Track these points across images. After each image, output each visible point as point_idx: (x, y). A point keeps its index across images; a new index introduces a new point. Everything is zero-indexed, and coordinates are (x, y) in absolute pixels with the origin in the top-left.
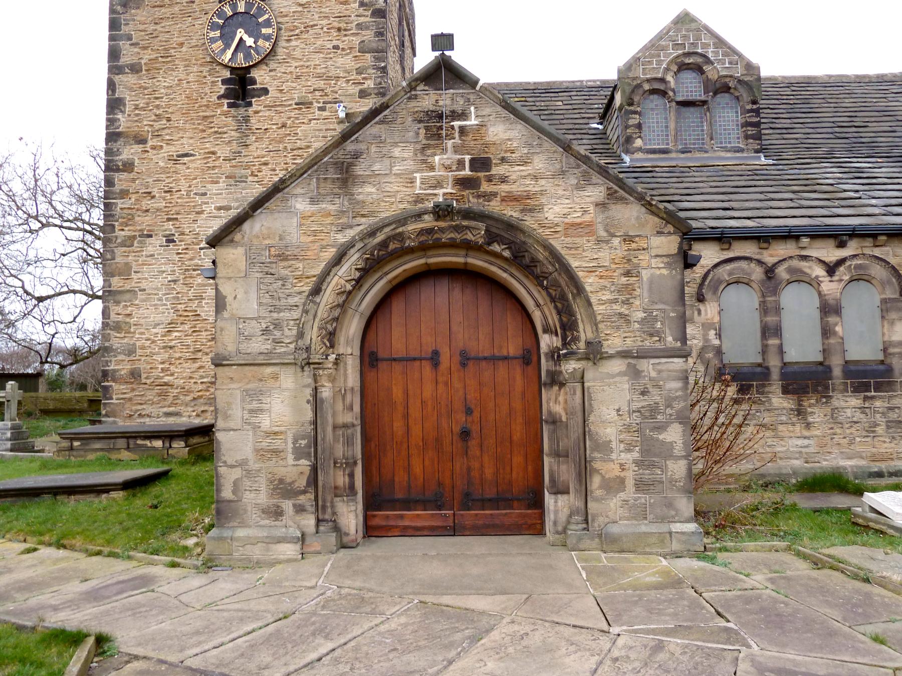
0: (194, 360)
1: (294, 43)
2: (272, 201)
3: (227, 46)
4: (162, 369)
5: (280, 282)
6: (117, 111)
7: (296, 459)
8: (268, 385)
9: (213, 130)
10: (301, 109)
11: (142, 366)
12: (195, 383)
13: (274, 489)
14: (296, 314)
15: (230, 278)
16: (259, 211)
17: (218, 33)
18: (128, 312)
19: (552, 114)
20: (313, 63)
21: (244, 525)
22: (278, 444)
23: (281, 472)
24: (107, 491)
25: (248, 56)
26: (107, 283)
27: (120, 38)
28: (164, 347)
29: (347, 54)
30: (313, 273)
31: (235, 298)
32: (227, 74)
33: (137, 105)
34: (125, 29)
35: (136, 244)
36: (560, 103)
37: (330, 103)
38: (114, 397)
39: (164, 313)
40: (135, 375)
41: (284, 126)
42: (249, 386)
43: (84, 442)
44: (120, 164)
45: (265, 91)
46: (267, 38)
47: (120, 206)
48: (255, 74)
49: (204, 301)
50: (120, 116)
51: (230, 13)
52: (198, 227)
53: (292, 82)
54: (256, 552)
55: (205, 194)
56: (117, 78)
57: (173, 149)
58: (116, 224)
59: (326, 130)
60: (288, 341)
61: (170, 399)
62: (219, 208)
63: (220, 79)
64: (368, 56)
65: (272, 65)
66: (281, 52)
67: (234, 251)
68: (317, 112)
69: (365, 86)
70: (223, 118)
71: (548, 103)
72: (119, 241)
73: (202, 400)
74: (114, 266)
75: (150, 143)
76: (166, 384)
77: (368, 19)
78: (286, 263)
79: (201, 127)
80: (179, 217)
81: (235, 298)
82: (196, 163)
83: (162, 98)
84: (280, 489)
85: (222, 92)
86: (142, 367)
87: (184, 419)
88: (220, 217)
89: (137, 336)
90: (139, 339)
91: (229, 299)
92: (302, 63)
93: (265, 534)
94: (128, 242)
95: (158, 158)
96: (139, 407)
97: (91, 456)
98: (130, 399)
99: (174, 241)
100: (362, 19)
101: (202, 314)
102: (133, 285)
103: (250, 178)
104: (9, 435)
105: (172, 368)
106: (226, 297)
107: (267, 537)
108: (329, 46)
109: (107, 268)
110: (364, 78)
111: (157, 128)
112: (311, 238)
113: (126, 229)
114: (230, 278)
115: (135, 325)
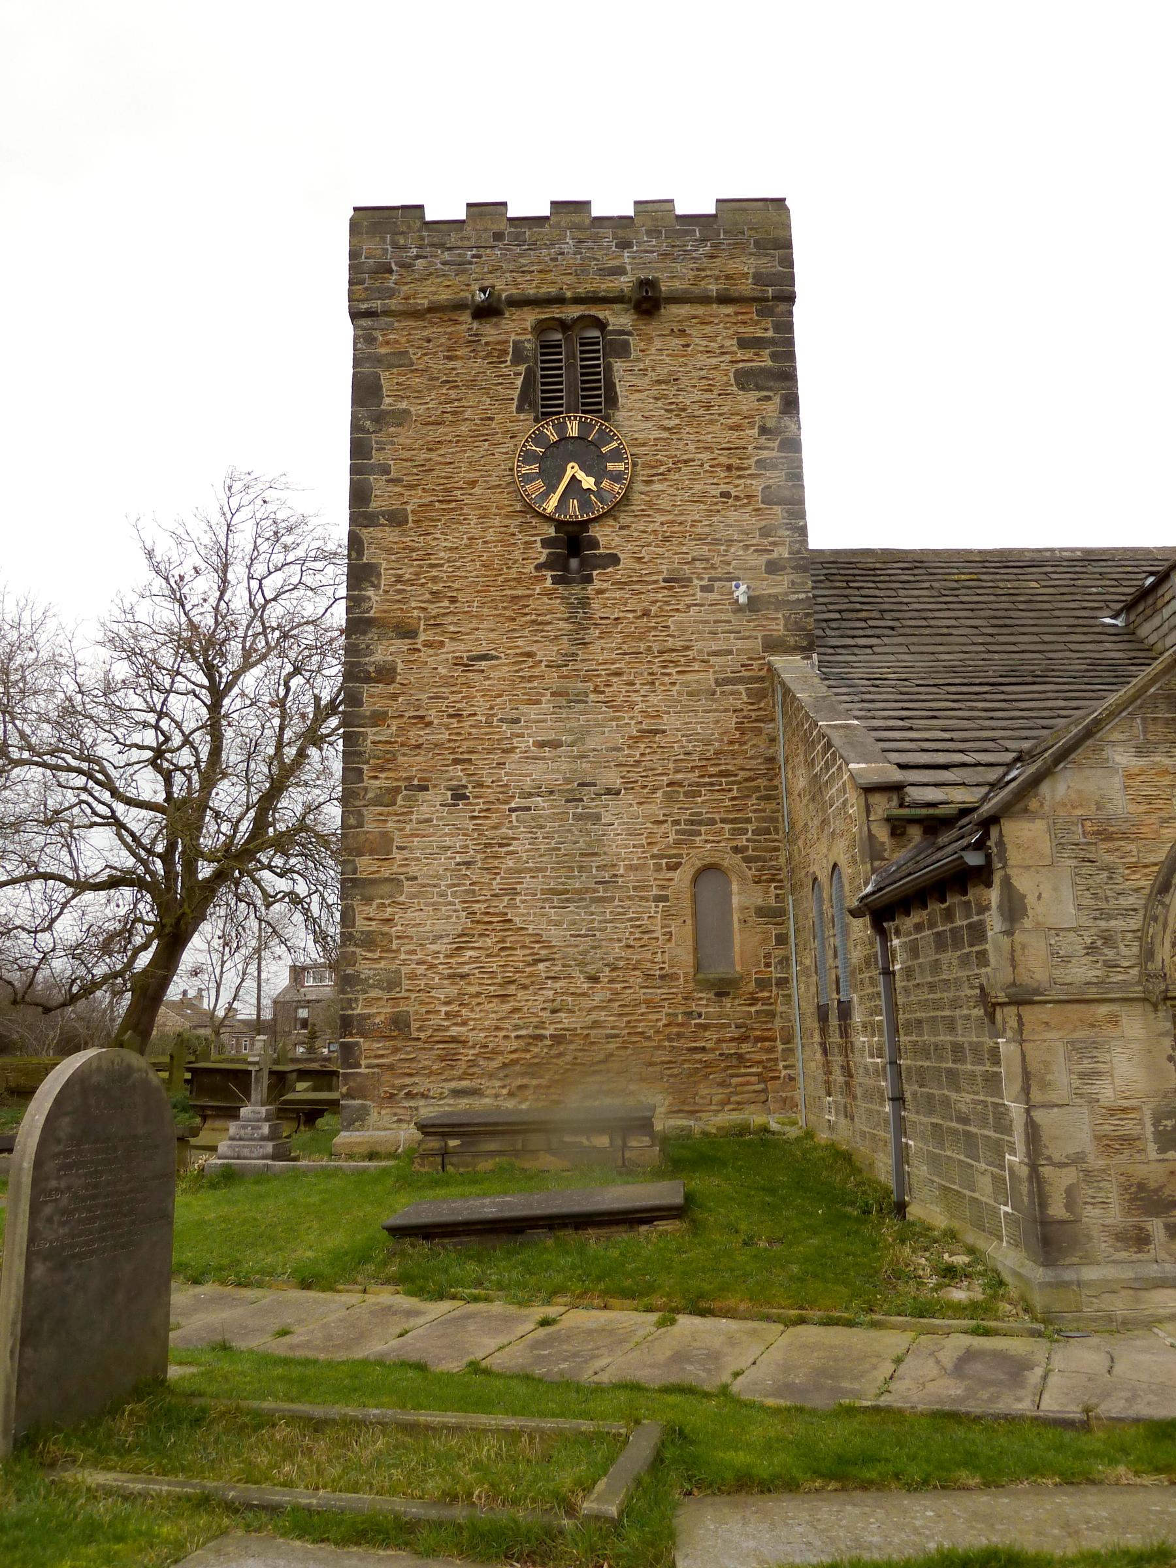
0: (504, 997)
1: (657, 487)
2: (1080, 750)
3: (552, 488)
4: (447, 1013)
5: (1105, 874)
6: (366, 585)
7: (1162, 1150)
8: (1105, 1033)
9: (528, 618)
10: (672, 588)
11: (412, 1008)
12: (506, 1037)
13: (1130, 1200)
14: (1134, 923)
15: (1028, 867)
16: (1062, 765)
17: (535, 468)
18: (387, 916)
19: (1030, 601)
20: (689, 518)
21: (1089, 1260)
22: (1129, 1127)
23: (1141, 1172)
24: (648, 1221)
25: (585, 505)
26: (349, 868)
27: (371, 470)
28: (451, 976)
29: (744, 505)
30: (1152, 860)
31: (1039, 897)
32: (551, 531)
33: (400, 576)
34: (377, 457)
35: (400, 801)
36: (1034, 584)
37: (720, 580)
38: (363, 1062)
39: (450, 917)
40: (399, 1023)
41: (646, 614)
42: (1076, 1035)
43: (467, 1139)
44: (372, 669)
45: (614, 560)
46: (617, 477)
47: (371, 738)
48: (596, 531)
49: (518, 898)
50: (370, 593)
51: (554, 438)
52: (507, 774)
53: (657, 546)
54: (1119, 1306)
55: (517, 721)
56: (365, 533)
57: (462, 647)
58: (365, 767)
59: (716, 622)
60: (1126, 964)
61: (462, 1065)
62: (541, 745)
63: (538, 538)
64: (778, 509)
65: (624, 519)
66: (636, 497)
67: (1031, 826)
68: (699, 594)
69: (775, 555)
70: (545, 599)
71: (1016, 584)
72: (370, 795)
73: (517, 1068)
74: (362, 838)
75: (422, 637)
76: (454, 1040)
77: (774, 454)
78: (1110, 845)
79: (508, 613)
80: (473, 757)
81: (1039, 897)
82: (499, 672)
83: (442, 565)
84: (1141, 1199)
85: (543, 558)
86: (411, 1010)
87: (487, 1101)
88: (543, 759)
89: (403, 956)
90: (406, 962)
91: (1031, 900)
92: (670, 518)
93: (1131, 1275)
94: (387, 797)
95: (436, 662)
96: (408, 1080)
97: (485, 1165)
98: (391, 1067)
99: (466, 798)
100: (765, 454)
101: (517, 920)
102: (395, 869)
103: (592, 697)
104: (265, 1129)
105: (464, 1012)
106: (1024, 896)
107: (1136, 1279)
108: (714, 493)
109: (350, 841)
110: (772, 544)
111: (434, 613)
112: (1143, 808)
113: (383, 775)
114: (1028, 867)
115: (399, 937)
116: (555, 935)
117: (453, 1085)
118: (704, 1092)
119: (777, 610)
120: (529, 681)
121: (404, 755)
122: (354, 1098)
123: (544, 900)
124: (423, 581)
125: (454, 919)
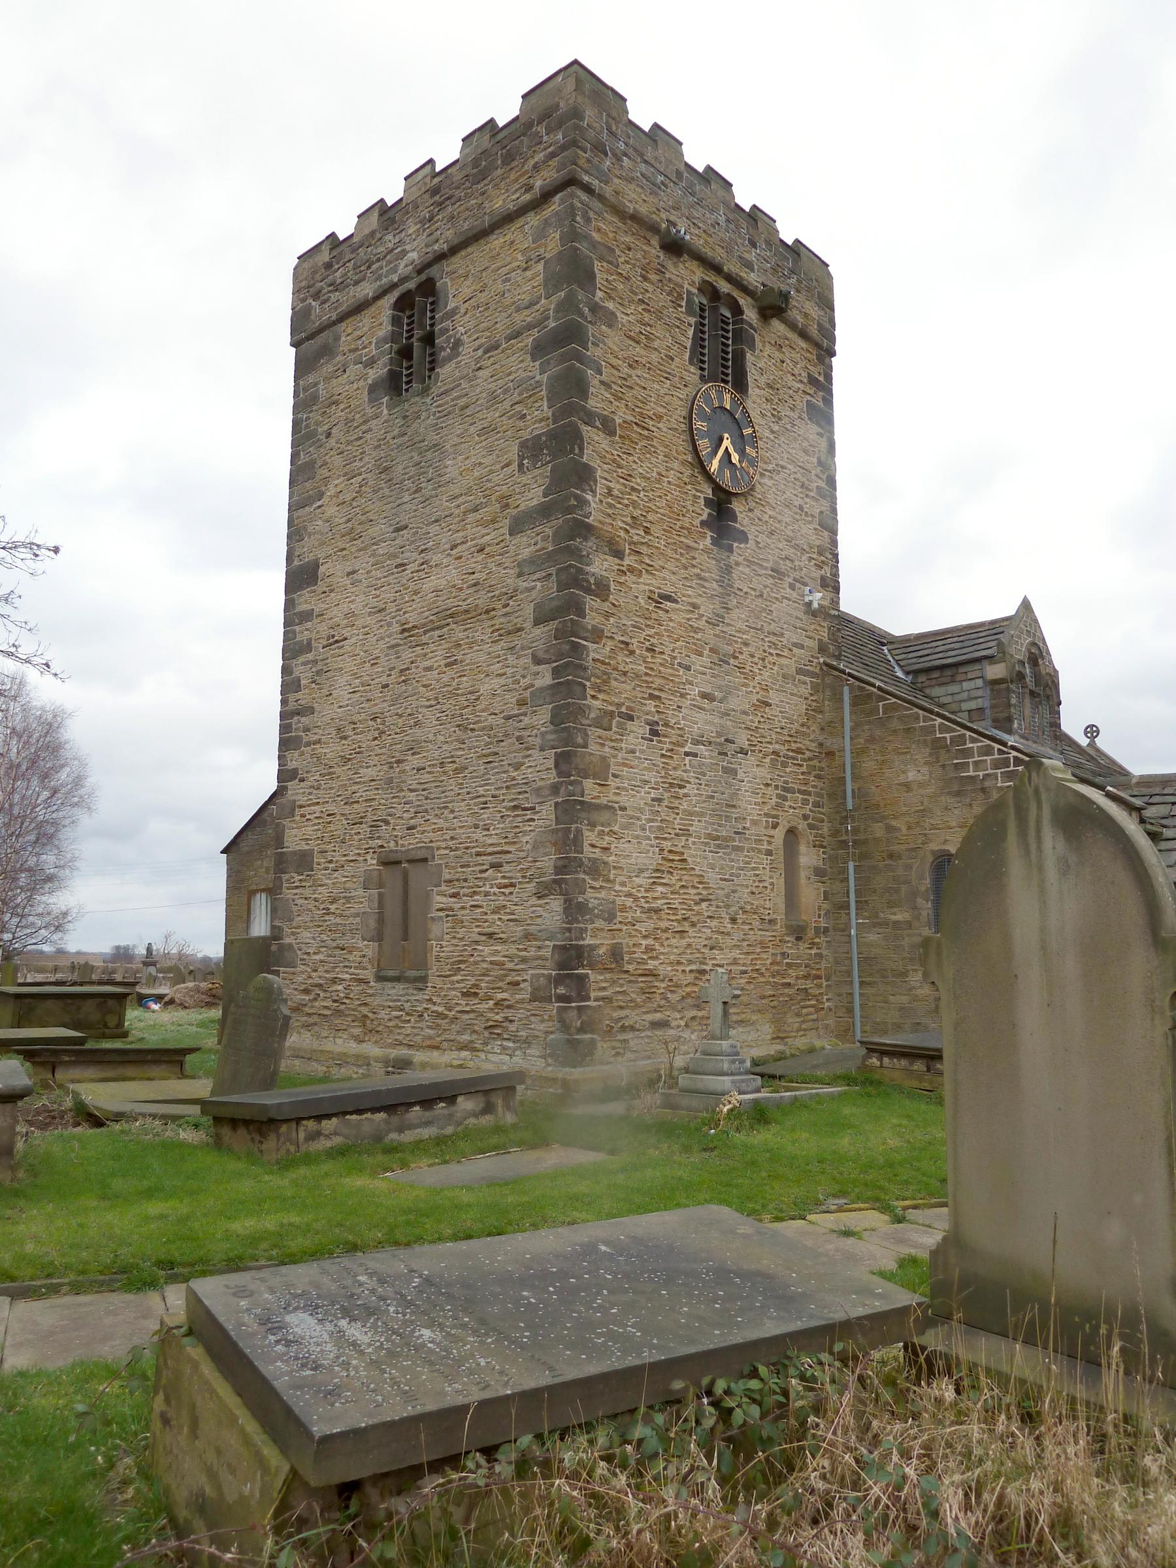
18: (605, 845)
38: (592, 995)
40: (616, 954)
49: (691, 839)
58: (588, 684)
80: (663, 695)
113: (600, 696)
116: (712, 877)
117: (650, 1017)
118: (790, 1020)
119: (824, 620)
120: (695, 632)
121: (616, 679)
122: (586, 1033)
123: (706, 844)
124: (626, 502)
125: (650, 855)
